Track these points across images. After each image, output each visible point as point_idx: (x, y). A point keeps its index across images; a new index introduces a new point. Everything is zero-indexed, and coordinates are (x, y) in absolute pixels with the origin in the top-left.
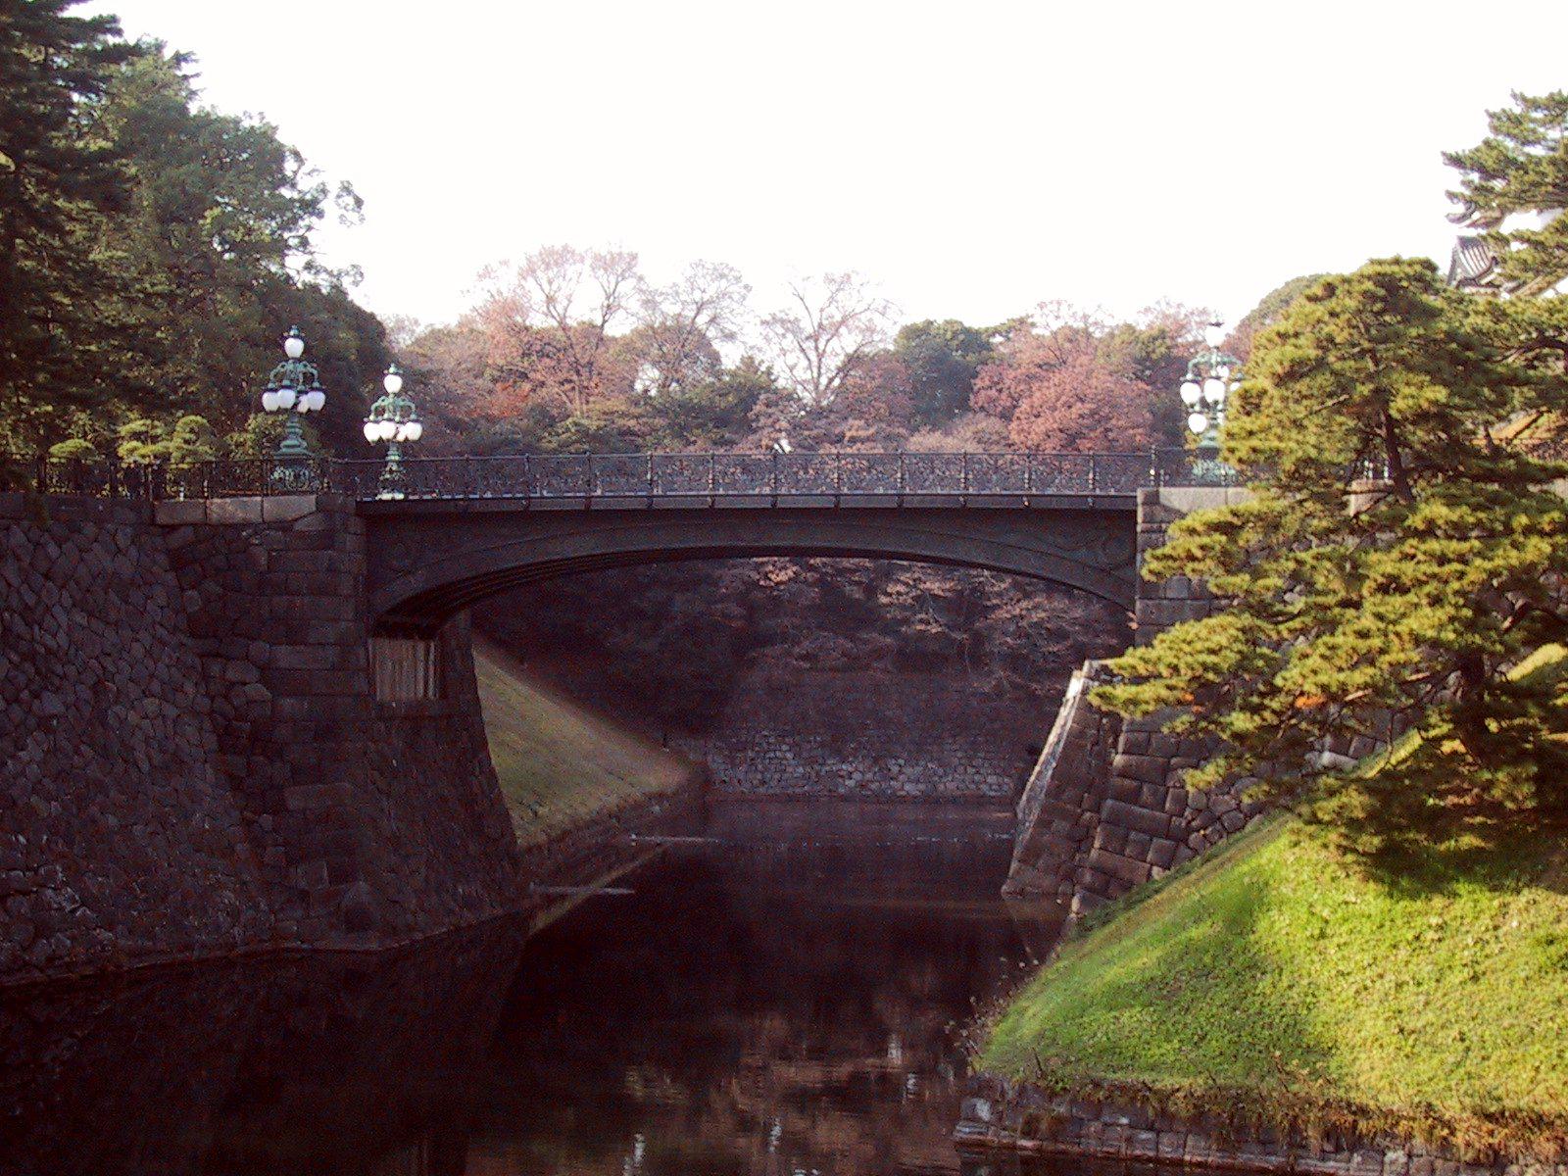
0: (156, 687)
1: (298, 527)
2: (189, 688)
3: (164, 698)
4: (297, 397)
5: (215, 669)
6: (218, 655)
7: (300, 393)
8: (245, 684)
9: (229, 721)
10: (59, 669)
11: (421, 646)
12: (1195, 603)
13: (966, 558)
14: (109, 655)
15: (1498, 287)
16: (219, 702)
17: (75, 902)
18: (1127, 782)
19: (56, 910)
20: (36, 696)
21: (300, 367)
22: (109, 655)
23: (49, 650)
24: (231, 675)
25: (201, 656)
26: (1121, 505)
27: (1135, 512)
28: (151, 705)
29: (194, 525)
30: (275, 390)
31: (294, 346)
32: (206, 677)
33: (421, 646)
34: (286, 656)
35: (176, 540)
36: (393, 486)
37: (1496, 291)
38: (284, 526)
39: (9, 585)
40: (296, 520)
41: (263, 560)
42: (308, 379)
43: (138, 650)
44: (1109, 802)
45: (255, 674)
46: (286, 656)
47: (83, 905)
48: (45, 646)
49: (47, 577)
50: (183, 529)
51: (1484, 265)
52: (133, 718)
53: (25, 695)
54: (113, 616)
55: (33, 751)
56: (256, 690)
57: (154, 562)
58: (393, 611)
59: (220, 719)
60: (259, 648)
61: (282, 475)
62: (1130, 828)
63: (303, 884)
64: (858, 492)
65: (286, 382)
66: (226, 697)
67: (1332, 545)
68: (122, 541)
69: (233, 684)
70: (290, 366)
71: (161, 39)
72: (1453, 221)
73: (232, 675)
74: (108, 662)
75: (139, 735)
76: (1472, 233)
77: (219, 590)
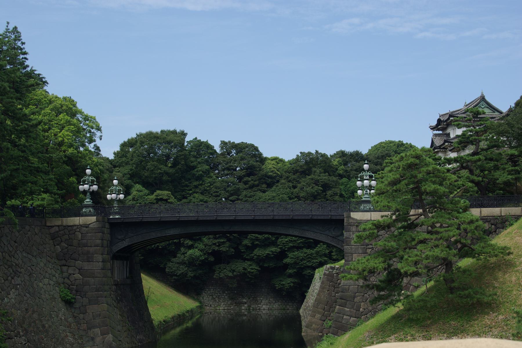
0: (47, 275)
1: (91, 226)
2: (57, 275)
3: (50, 279)
4: (90, 187)
5: (65, 268)
6: (65, 266)
7: (90, 186)
8: (74, 274)
9: (69, 286)
10: (19, 270)
11: (125, 262)
12: (362, 246)
13: (292, 234)
14: (34, 266)
15: (447, 149)
16: (66, 280)
17: (26, 341)
18: (343, 301)
19: (20, 343)
20: (13, 278)
21: (91, 178)
22: (34, 266)
23: (16, 265)
24: (70, 272)
25: (60, 266)
26: (338, 218)
27: (343, 220)
28: (46, 281)
29: (58, 226)
30: (83, 185)
31: (88, 171)
32: (62, 272)
33: (125, 262)
34: (86, 266)
35: (53, 230)
36: (116, 213)
37: (446, 150)
38: (87, 226)
39: (5, 245)
40: (90, 224)
41: (80, 236)
42: (93, 181)
43: (42, 264)
44: (338, 307)
45: (77, 271)
46: (86, 266)
47: (28, 342)
48: (15, 263)
49: (15, 242)
50: (55, 227)
51: (442, 143)
52: (41, 284)
53: (10, 278)
54: (35, 254)
55: (13, 294)
56: (78, 276)
57: (46, 237)
58: (118, 252)
59: (67, 285)
60: (79, 263)
61: (85, 211)
62: (344, 315)
63: (92, 336)
64: (279, 214)
65: (86, 182)
66: (68, 278)
67: (350, 275)
68: (36, 231)
69: (70, 274)
70: (87, 178)
71: (182, 130)
72: (431, 129)
73: (71, 271)
74: (33, 268)
75: (43, 290)
76: (438, 132)
77: (66, 246)
